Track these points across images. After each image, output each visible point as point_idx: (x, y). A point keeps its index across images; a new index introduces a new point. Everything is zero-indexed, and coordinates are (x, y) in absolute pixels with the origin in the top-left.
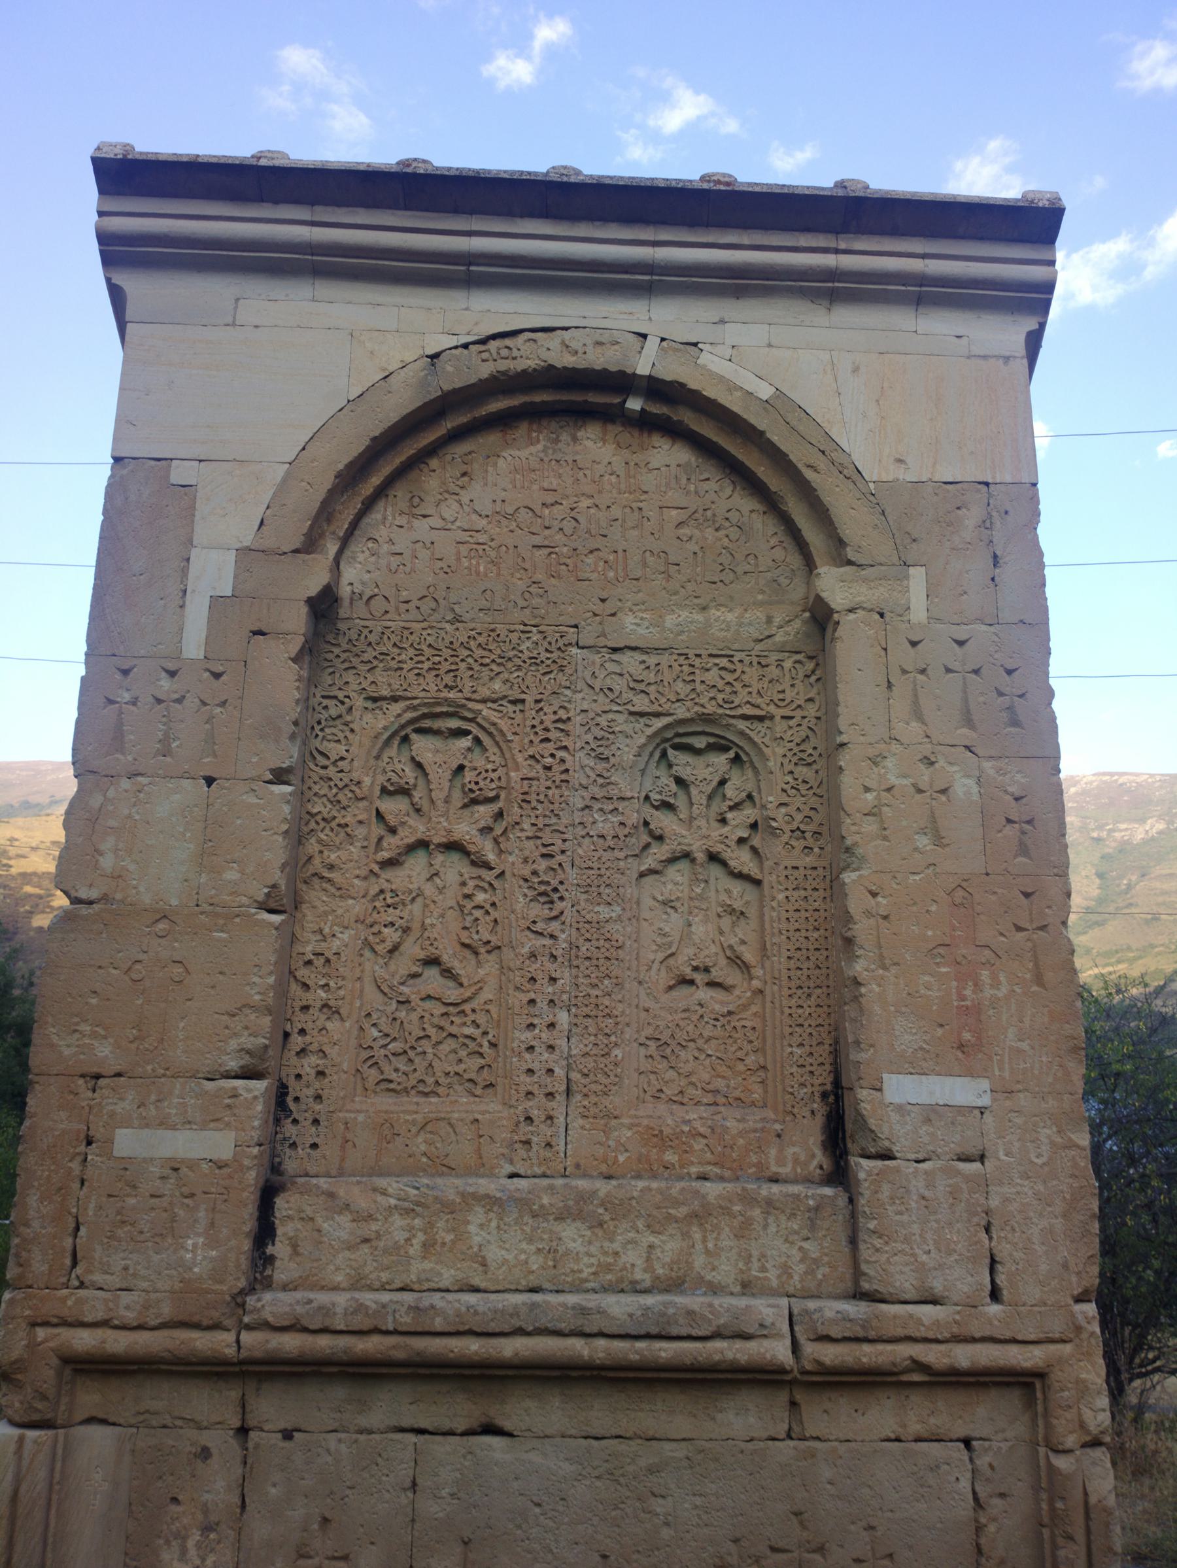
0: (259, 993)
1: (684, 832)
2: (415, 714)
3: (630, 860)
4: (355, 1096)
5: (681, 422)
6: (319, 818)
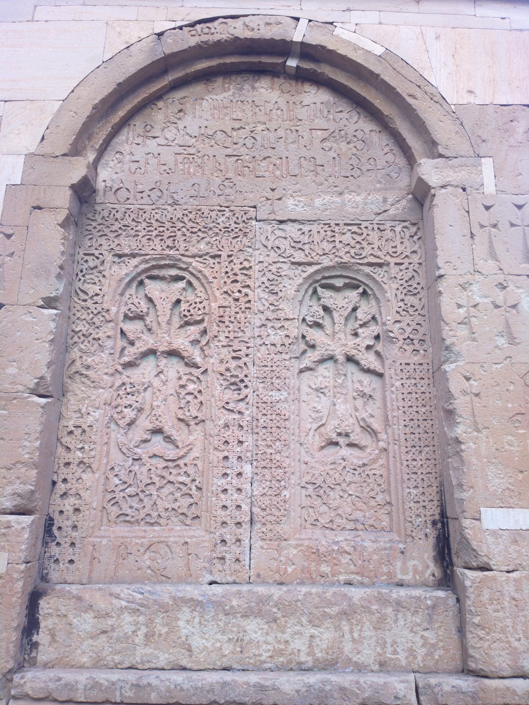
0: (28, 453)
1: (329, 343)
2: (147, 266)
3: (293, 360)
5: (323, 74)
6: (80, 334)
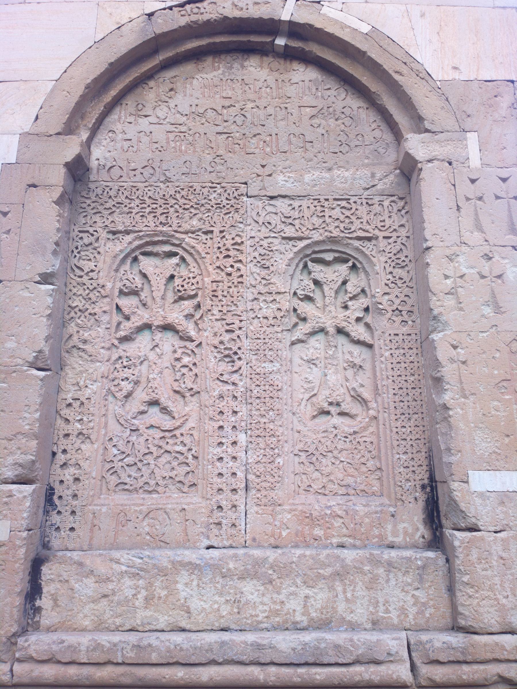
0: (28, 424)
1: (320, 315)
2: (141, 242)
3: (285, 333)
4: (101, 494)
5: (310, 52)
6: (77, 310)
